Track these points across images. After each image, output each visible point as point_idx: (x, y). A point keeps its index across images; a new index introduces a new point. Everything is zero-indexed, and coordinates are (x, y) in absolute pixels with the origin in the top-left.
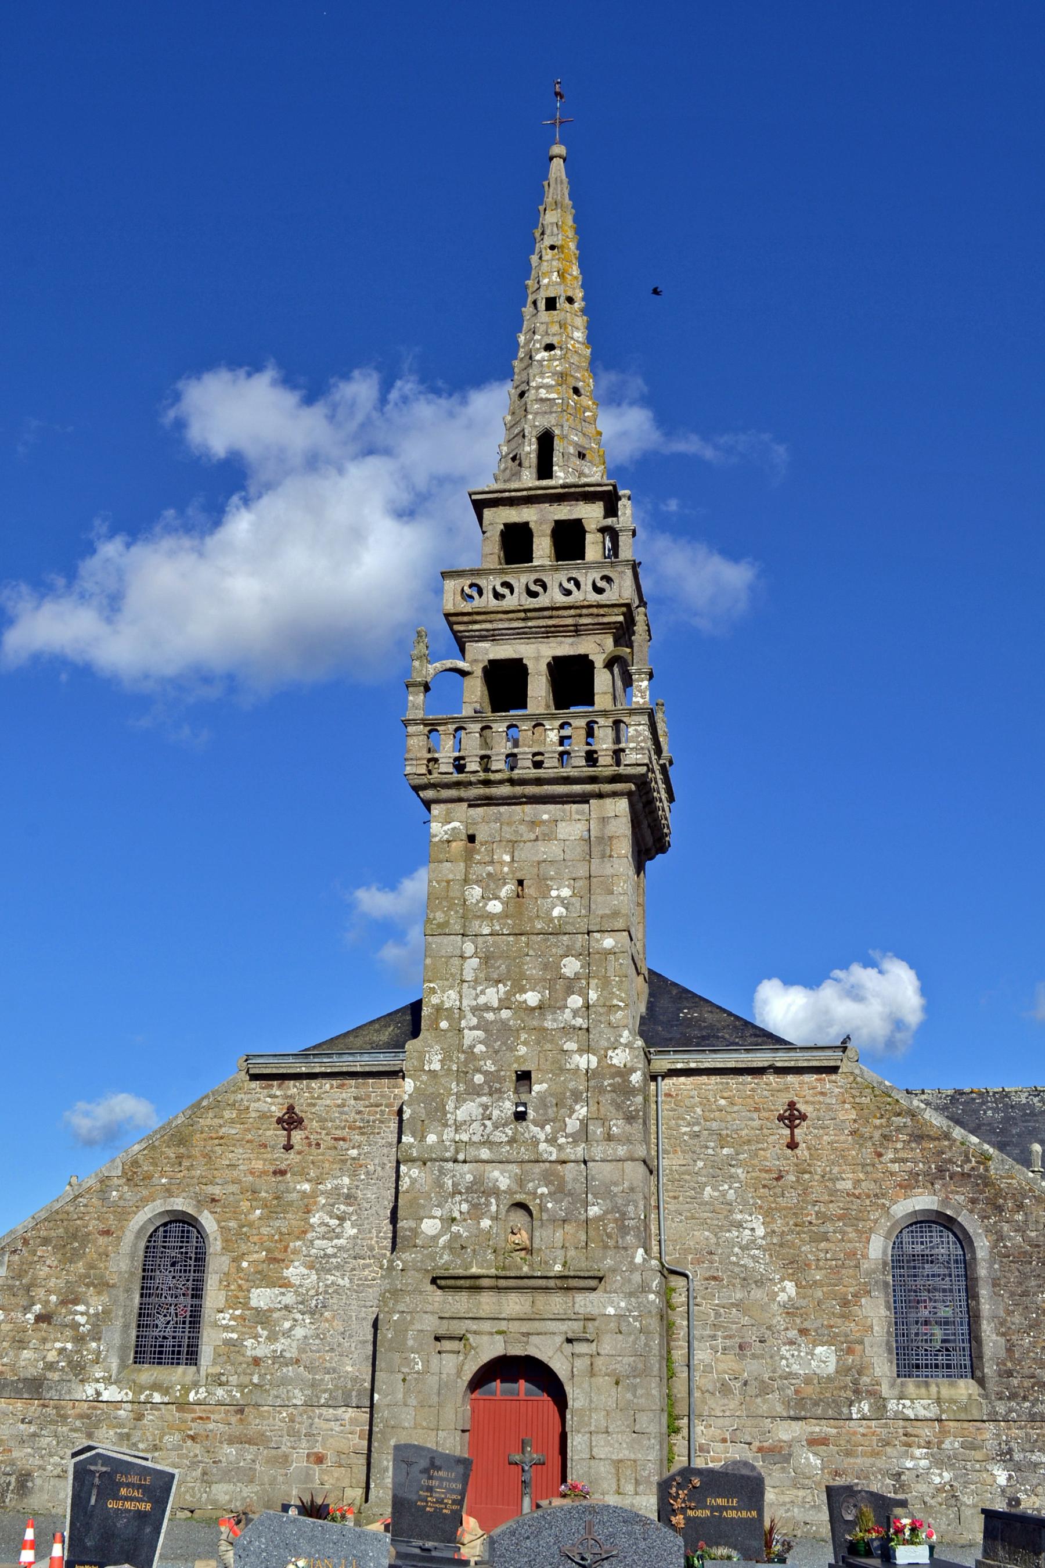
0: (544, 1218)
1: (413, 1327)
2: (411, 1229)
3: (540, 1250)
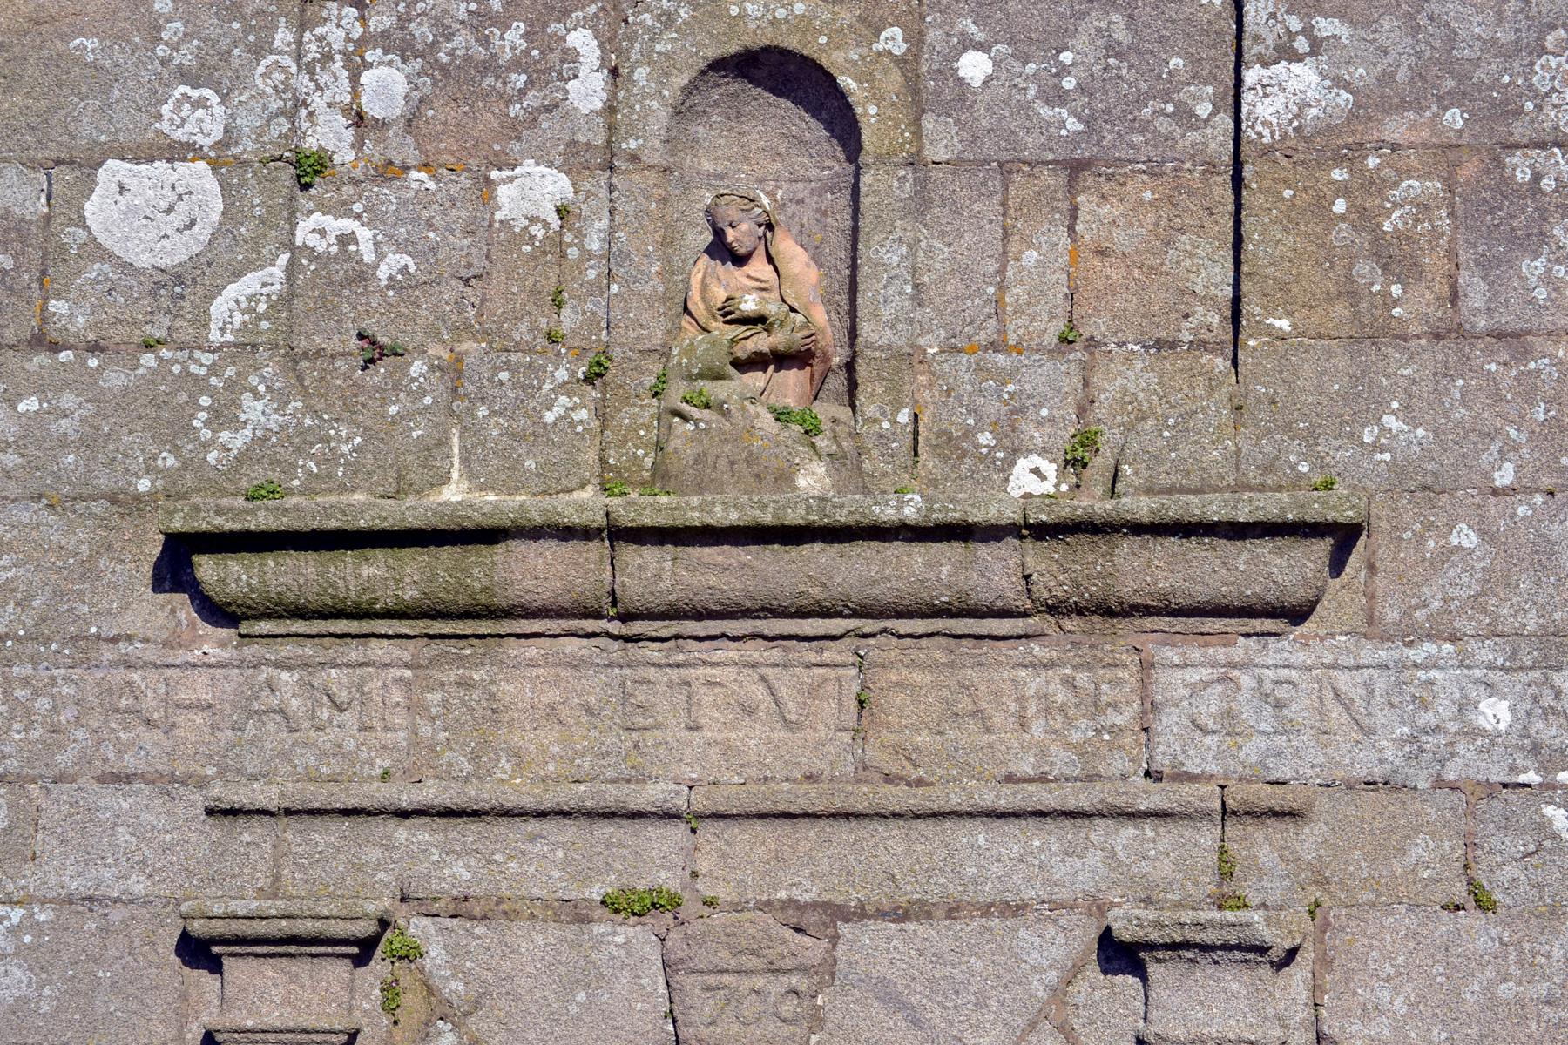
0: (936, 151)
1: (30, 879)
3: (909, 358)
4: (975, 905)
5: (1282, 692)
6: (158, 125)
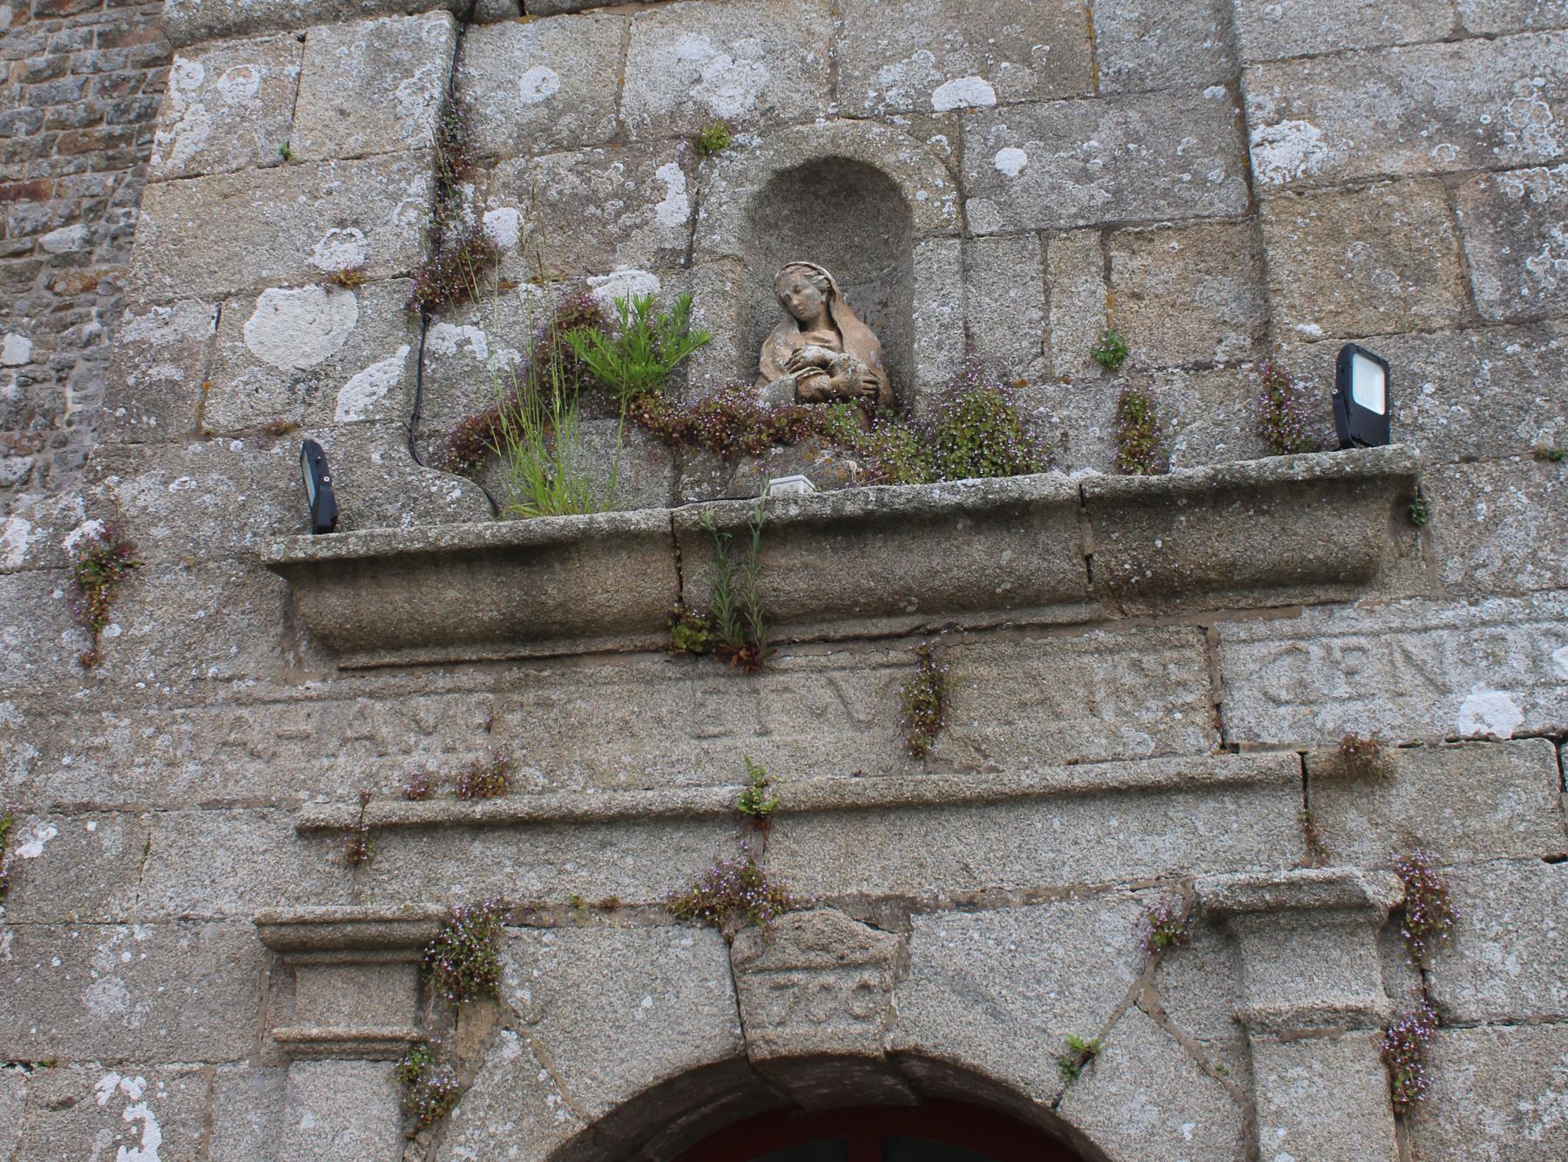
2: (180, 352)
4: (1054, 890)
5: (1352, 660)
6: (311, 260)
